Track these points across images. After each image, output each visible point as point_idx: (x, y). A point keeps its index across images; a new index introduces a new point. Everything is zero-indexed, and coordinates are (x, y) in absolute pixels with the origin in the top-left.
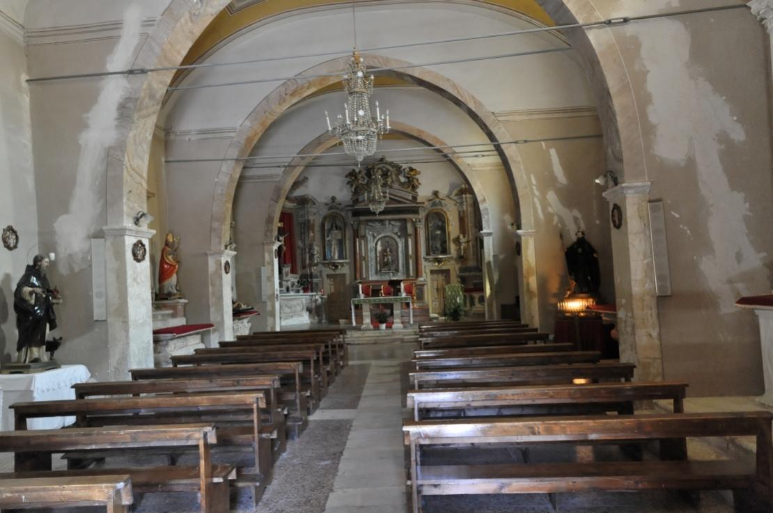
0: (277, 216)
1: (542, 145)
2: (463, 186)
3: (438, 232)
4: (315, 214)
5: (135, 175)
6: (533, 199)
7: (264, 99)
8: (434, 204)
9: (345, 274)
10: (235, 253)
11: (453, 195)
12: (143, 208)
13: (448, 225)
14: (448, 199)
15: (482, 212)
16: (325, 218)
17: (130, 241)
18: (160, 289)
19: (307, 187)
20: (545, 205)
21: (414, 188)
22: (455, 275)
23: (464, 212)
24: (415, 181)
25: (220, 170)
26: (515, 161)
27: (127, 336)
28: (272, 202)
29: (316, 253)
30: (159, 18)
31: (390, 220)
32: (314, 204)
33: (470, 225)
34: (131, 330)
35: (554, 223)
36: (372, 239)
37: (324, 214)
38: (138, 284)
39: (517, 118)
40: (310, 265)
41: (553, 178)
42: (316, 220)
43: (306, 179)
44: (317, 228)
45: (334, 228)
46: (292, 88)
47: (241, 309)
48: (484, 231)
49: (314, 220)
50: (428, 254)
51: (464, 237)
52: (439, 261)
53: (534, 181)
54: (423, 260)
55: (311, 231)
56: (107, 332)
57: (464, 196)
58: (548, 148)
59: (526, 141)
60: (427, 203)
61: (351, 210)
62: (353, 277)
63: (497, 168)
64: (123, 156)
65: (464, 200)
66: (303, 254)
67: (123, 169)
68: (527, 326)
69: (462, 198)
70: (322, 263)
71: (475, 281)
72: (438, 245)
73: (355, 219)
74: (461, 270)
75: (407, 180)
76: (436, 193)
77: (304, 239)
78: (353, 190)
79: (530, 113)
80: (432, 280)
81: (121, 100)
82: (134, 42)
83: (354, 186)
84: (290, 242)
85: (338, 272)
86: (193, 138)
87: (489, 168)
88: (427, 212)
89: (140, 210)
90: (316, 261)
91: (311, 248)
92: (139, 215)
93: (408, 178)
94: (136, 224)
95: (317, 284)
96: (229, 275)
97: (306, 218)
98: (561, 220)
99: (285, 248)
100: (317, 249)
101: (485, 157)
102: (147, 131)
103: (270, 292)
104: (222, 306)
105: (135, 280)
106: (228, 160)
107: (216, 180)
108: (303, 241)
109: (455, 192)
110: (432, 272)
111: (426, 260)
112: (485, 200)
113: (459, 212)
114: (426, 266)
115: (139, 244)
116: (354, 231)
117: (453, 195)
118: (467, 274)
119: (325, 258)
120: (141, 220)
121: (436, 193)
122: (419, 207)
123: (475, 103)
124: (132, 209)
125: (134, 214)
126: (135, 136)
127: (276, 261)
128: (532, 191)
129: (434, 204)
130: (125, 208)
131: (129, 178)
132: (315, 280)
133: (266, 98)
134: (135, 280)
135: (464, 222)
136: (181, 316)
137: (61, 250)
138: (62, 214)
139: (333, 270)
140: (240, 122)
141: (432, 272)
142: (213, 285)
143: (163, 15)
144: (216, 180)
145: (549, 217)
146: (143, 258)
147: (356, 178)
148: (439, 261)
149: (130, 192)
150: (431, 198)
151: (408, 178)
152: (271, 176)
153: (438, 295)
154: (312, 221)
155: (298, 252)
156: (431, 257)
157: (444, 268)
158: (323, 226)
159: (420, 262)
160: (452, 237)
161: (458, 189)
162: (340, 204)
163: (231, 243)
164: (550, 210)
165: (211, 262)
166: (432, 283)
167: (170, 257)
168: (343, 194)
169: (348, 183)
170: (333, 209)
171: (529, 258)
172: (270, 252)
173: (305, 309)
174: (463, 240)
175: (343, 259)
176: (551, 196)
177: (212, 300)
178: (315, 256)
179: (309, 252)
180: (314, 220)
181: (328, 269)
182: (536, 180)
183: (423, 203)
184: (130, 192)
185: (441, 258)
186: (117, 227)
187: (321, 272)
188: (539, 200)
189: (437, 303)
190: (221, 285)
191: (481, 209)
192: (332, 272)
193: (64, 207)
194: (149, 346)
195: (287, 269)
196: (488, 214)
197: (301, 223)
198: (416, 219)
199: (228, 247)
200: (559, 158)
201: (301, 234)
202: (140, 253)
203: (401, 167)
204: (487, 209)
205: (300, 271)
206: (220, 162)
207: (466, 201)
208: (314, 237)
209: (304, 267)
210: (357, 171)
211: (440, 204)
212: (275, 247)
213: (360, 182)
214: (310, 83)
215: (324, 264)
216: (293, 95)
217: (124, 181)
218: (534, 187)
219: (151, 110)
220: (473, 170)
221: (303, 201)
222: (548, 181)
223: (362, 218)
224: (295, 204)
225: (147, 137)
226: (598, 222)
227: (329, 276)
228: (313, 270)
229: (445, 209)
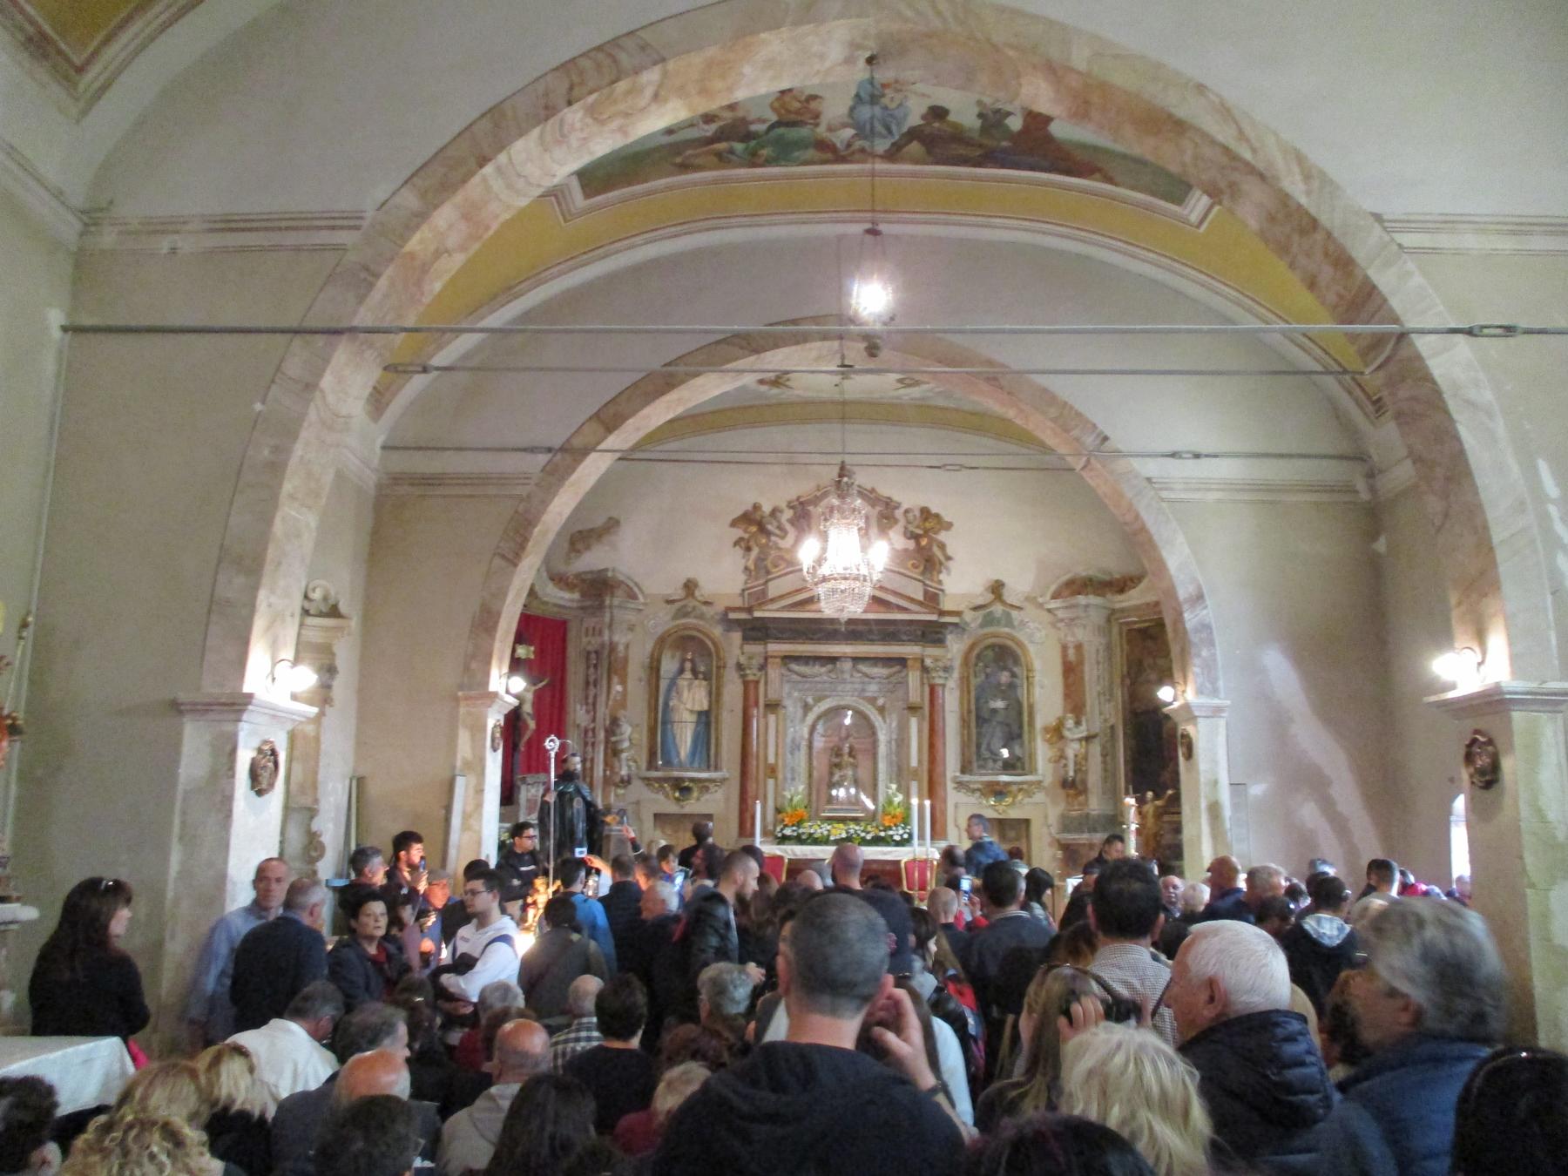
3: (999, 704)
4: (631, 628)
7: (483, 115)
8: (989, 620)
13: (1030, 684)
14: (1029, 607)
16: (661, 642)
22: (1047, 839)
24: (935, 549)
25: (278, 369)
26: (1470, 403)
28: (498, 561)
29: (626, 744)
31: (856, 660)
32: (634, 597)
36: (800, 712)
37: (660, 631)
39: (1470, 241)
43: (612, 525)
45: (688, 675)
49: (627, 647)
51: (1078, 723)
52: (998, 791)
53: (1551, 488)
55: (615, 679)
59: (1509, 330)
73: (755, 649)
74: (1067, 824)
76: (997, 588)
77: (594, 704)
79: (1521, 228)
86: (186, 245)
87: (1212, 496)
90: (624, 772)
91: (613, 726)
97: (606, 638)
101: (1203, 461)
107: (258, 407)
108: (593, 707)
111: (960, 785)
113: (1064, 648)
116: (746, 684)
121: (997, 588)
123: (1307, 177)
129: (989, 620)
133: (490, 110)
139: (677, 800)
140: (381, 194)
144: (258, 407)
147: (762, 529)
150: (980, 601)
152: (503, 480)
154: (621, 648)
157: (1014, 814)
158: (654, 668)
160: (1039, 723)
162: (706, 603)
165: (194, 739)
170: (686, 615)
172: (478, 728)
174: (1073, 732)
178: (624, 755)
179: (607, 741)
180: (627, 647)
181: (661, 797)
183: (958, 614)
191: (1189, 626)
192: (672, 808)
196: (1211, 643)
201: (587, 683)
206: (280, 339)
208: (624, 693)
210: (767, 509)
211: (1009, 622)
215: (648, 781)
220: (1163, 500)
221: (598, 588)
223: (775, 648)
224: (576, 596)
228: (612, 798)
229: (1021, 636)
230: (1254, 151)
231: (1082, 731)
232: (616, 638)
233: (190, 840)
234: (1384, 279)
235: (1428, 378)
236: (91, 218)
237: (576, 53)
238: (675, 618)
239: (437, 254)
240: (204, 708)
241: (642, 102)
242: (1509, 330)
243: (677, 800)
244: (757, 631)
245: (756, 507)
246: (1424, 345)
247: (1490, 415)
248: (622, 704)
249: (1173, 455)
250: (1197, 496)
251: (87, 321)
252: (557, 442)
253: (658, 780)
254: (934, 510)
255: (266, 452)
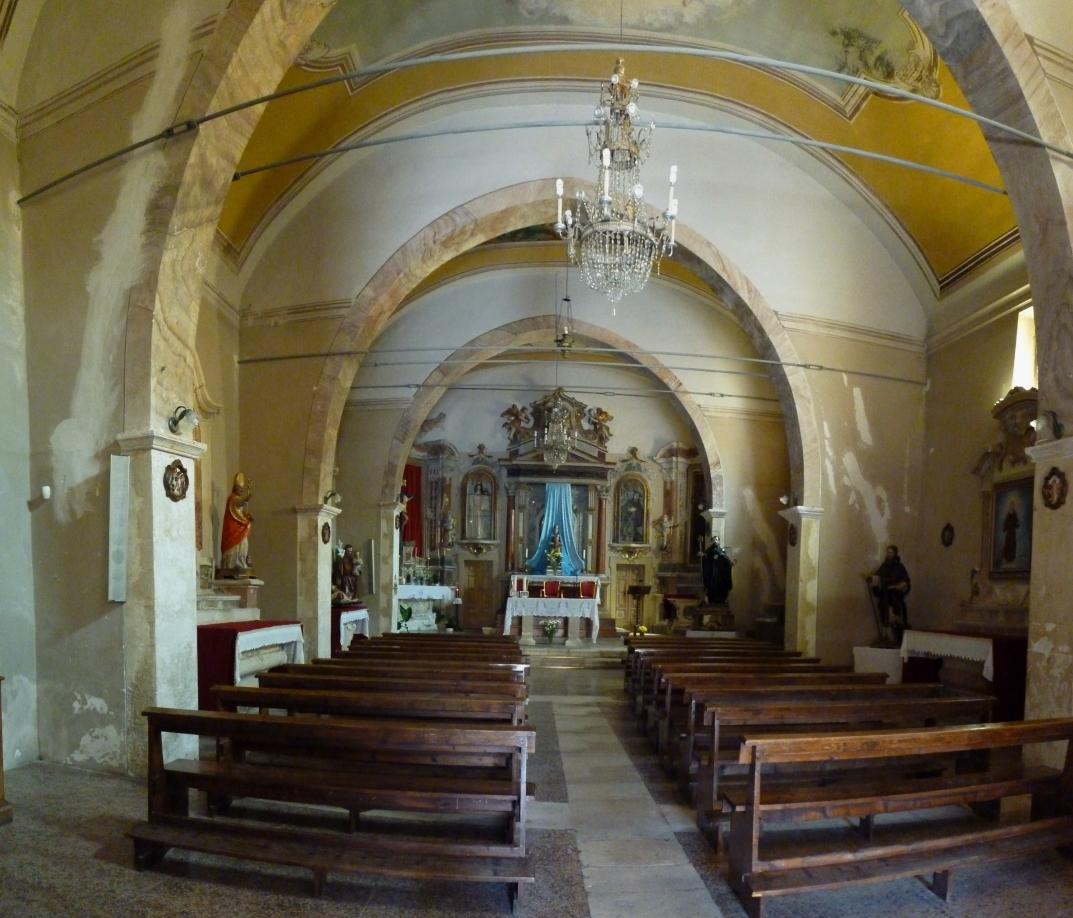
0: (400, 471)
1: (842, 379)
2: (675, 445)
3: (633, 509)
4: (452, 470)
5: (173, 338)
6: (823, 461)
9: (491, 562)
10: (339, 511)
11: (659, 456)
12: (184, 401)
14: (650, 462)
15: (714, 481)
16: (467, 477)
17: (159, 461)
18: (222, 562)
19: (443, 429)
20: (840, 473)
21: (602, 440)
23: (672, 483)
26: (802, 396)
27: (152, 633)
28: (395, 442)
29: (451, 527)
30: (223, 13)
32: (453, 454)
33: (679, 503)
34: (157, 621)
35: (850, 502)
37: (466, 471)
38: (173, 540)
39: (811, 329)
40: (442, 546)
41: (854, 435)
42: (456, 481)
43: (442, 416)
44: (455, 491)
46: (446, 231)
47: (342, 601)
48: (714, 510)
49: (450, 479)
50: (615, 540)
51: (670, 519)
52: (631, 551)
54: (607, 548)
55: (445, 495)
56: (122, 622)
57: (674, 459)
58: (852, 384)
59: (821, 368)
60: (619, 465)
61: (506, 466)
62: (503, 567)
63: (742, 417)
64: (153, 301)
65: (674, 465)
66: (433, 528)
67: (152, 324)
68: (799, 654)
69: (671, 462)
70: (459, 544)
71: (680, 585)
72: (631, 529)
73: (512, 480)
74: (663, 567)
75: (592, 428)
76: (633, 451)
78: (512, 436)
79: (832, 325)
80: (619, 579)
81: (153, 196)
82: (178, 74)
83: (514, 430)
84: (414, 509)
85: (481, 557)
86: (281, 322)
87: (729, 415)
88: (618, 477)
89: (181, 404)
91: (444, 520)
92: (178, 415)
93: (595, 424)
94: (173, 431)
95: (450, 574)
96: (329, 546)
98: (860, 499)
99: (407, 518)
100: (453, 522)
101: (725, 398)
102: (197, 256)
103: (388, 581)
104: (315, 594)
105: (168, 532)
106: (334, 354)
107: (315, 388)
109: (661, 452)
110: (620, 567)
111: (612, 548)
112: (718, 463)
113: (665, 483)
114: (612, 558)
115: (175, 470)
116: (509, 497)
117: (659, 456)
118: (669, 574)
119: (463, 536)
120: (181, 423)
121: (633, 451)
122: (607, 469)
123: (750, 291)
124: (166, 401)
125: (169, 410)
126: (174, 262)
127: (397, 533)
128: (823, 446)
129: (629, 468)
130: (154, 400)
131: (162, 345)
132: (447, 568)
134: (168, 532)
135: (671, 498)
136: (253, 607)
137: (59, 481)
138: (56, 423)
139: (475, 554)
141: (620, 567)
142: (303, 560)
143: (228, 8)
144: (315, 388)
145: (844, 491)
146: (183, 496)
148: (631, 551)
149: (163, 369)
150: (626, 458)
151: (595, 424)
153: (625, 601)
155: (426, 524)
156: (620, 545)
157: (637, 562)
159: (602, 552)
160: (651, 519)
161: (667, 447)
162: (490, 457)
163: (333, 494)
164: (846, 480)
165: (302, 523)
166: (618, 583)
167: (239, 511)
168: (497, 442)
169: (505, 425)
170: (479, 463)
171: (810, 552)
172: (389, 519)
173: (431, 610)
174: (667, 523)
175: (490, 539)
176: (850, 460)
177: (300, 584)
178: (450, 532)
180: (450, 479)
181: (467, 552)
182: (831, 432)
183: (614, 464)
184: (163, 369)
185: (635, 548)
186: (138, 433)
187: (456, 556)
188: (832, 463)
189: (623, 612)
190: (315, 561)
192: (472, 558)
193: (65, 412)
194: (190, 653)
195: (409, 549)
197: (432, 483)
198: (602, 487)
199: (330, 500)
200: (866, 405)
201: (431, 498)
202: (178, 483)
203: (586, 406)
204: (721, 477)
205: (428, 553)
207: (677, 468)
209: (433, 548)
210: (519, 408)
211: (639, 467)
212: (396, 513)
213: (523, 424)
214: (476, 225)
215: (462, 545)
216: (445, 244)
217: (153, 348)
218: (827, 442)
219: (206, 213)
221: (437, 449)
222: (847, 437)
223: (522, 479)
225: (195, 269)
226: (907, 509)
227: (468, 563)
229: (644, 476)
230: (728, 276)
231: (672, 523)
232: (445, 475)
233: (303, 560)
234: (775, 340)
235: (786, 384)
236: (244, 314)
237: (437, 217)
238: (473, 464)
239: (380, 314)
240: (306, 511)
241: (466, 237)
242: (821, 368)
243: (475, 554)
244: (515, 472)
245: (514, 406)
246: (787, 370)
247: (809, 402)
248: (448, 507)
249: (711, 394)
250: (719, 415)
251: (247, 358)
252: (421, 383)
253: (466, 544)
254: (604, 410)
255: (319, 407)
